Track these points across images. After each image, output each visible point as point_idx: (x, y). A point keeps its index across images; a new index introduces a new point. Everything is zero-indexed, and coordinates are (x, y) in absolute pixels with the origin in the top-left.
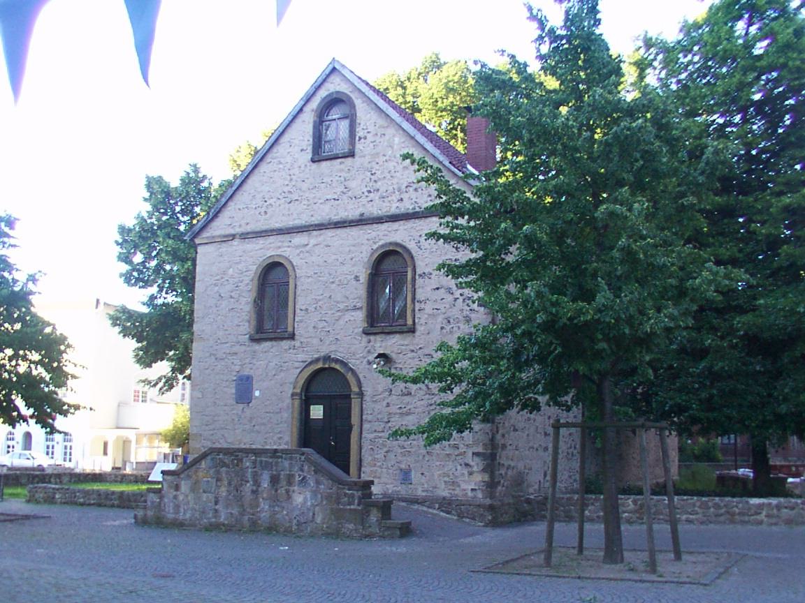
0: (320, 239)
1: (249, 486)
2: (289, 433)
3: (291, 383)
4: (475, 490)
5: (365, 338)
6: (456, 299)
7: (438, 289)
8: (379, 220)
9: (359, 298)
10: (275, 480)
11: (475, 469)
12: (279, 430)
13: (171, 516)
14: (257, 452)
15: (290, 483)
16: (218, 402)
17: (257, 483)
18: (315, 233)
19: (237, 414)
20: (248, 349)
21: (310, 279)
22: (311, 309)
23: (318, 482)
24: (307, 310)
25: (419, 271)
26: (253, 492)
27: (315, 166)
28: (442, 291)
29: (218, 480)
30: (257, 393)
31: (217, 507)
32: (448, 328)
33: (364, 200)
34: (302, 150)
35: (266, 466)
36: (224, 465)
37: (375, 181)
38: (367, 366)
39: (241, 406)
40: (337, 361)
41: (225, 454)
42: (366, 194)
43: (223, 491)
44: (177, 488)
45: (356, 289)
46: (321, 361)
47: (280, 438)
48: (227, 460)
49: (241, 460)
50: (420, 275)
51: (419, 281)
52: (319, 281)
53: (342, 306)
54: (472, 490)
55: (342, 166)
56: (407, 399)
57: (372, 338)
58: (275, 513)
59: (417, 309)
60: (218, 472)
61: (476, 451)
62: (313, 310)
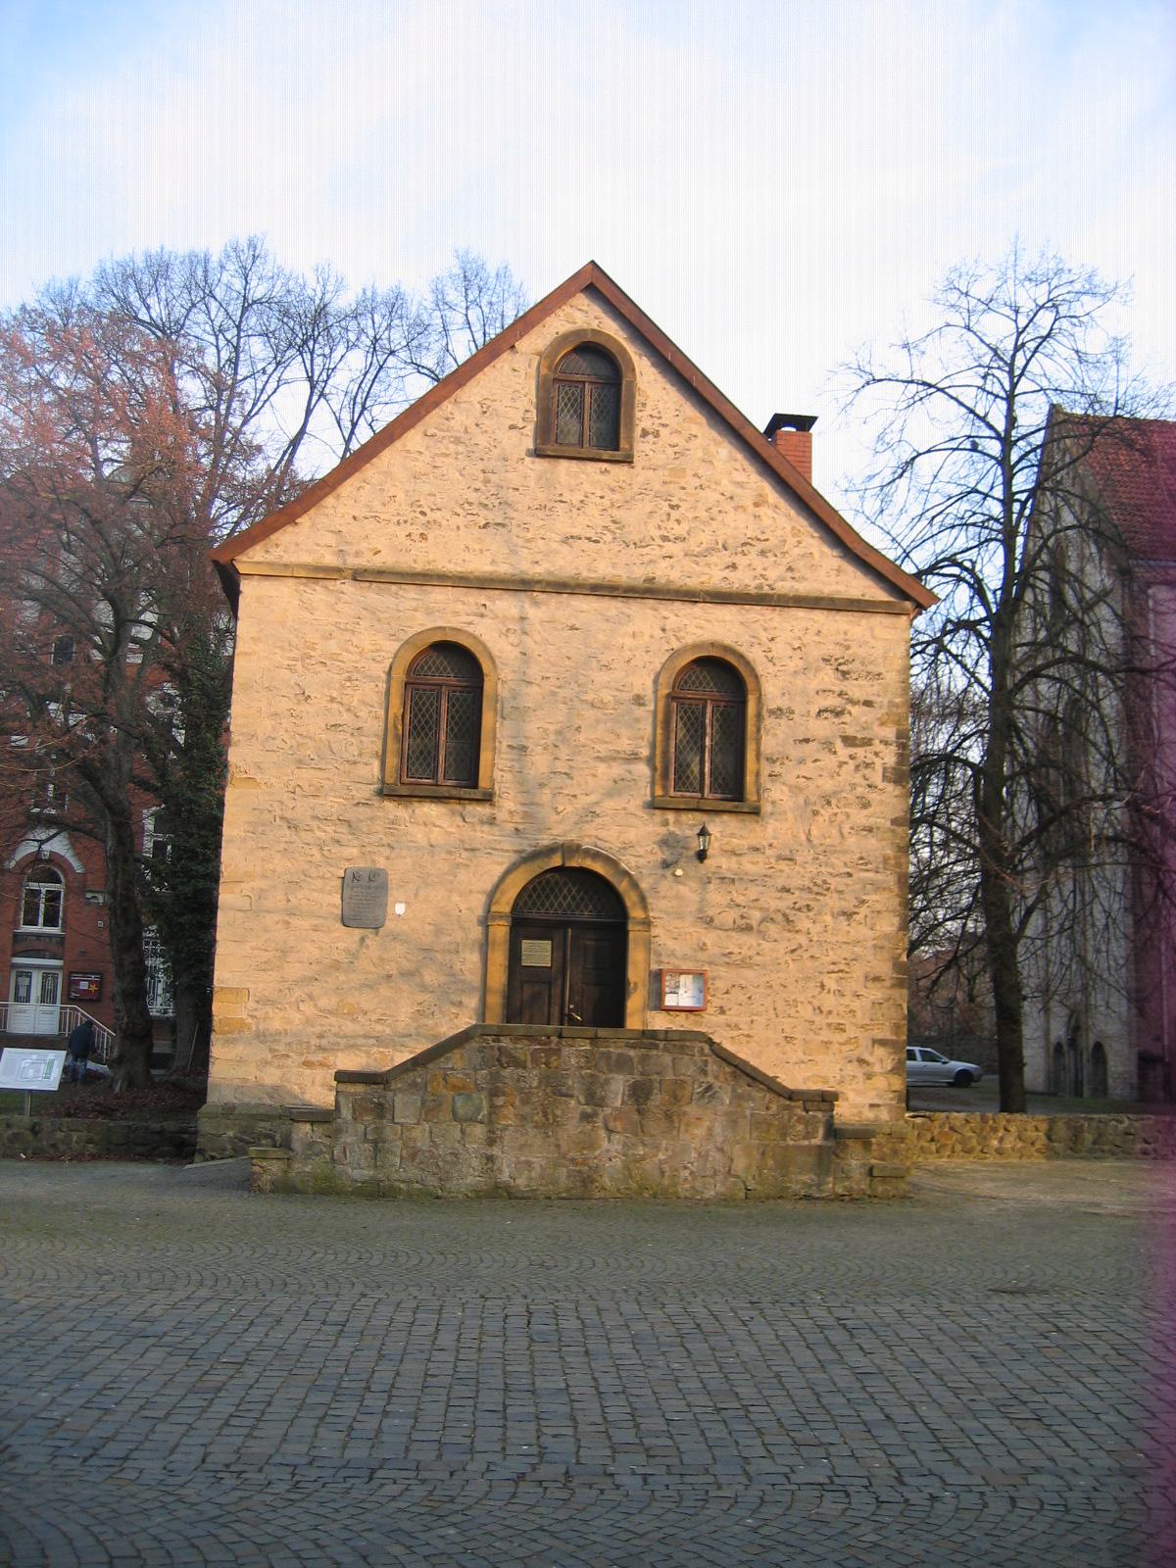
1: (575, 1106)
4: (878, 1106)
11: (877, 1068)
23: (738, 1098)
27: (541, 465)
31: (495, 1151)
34: (512, 427)
35: (622, 1064)
37: (678, 522)
49: (558, 1052)
50: (772, 712)
54: (872, 1106)
61: (880, 1036)
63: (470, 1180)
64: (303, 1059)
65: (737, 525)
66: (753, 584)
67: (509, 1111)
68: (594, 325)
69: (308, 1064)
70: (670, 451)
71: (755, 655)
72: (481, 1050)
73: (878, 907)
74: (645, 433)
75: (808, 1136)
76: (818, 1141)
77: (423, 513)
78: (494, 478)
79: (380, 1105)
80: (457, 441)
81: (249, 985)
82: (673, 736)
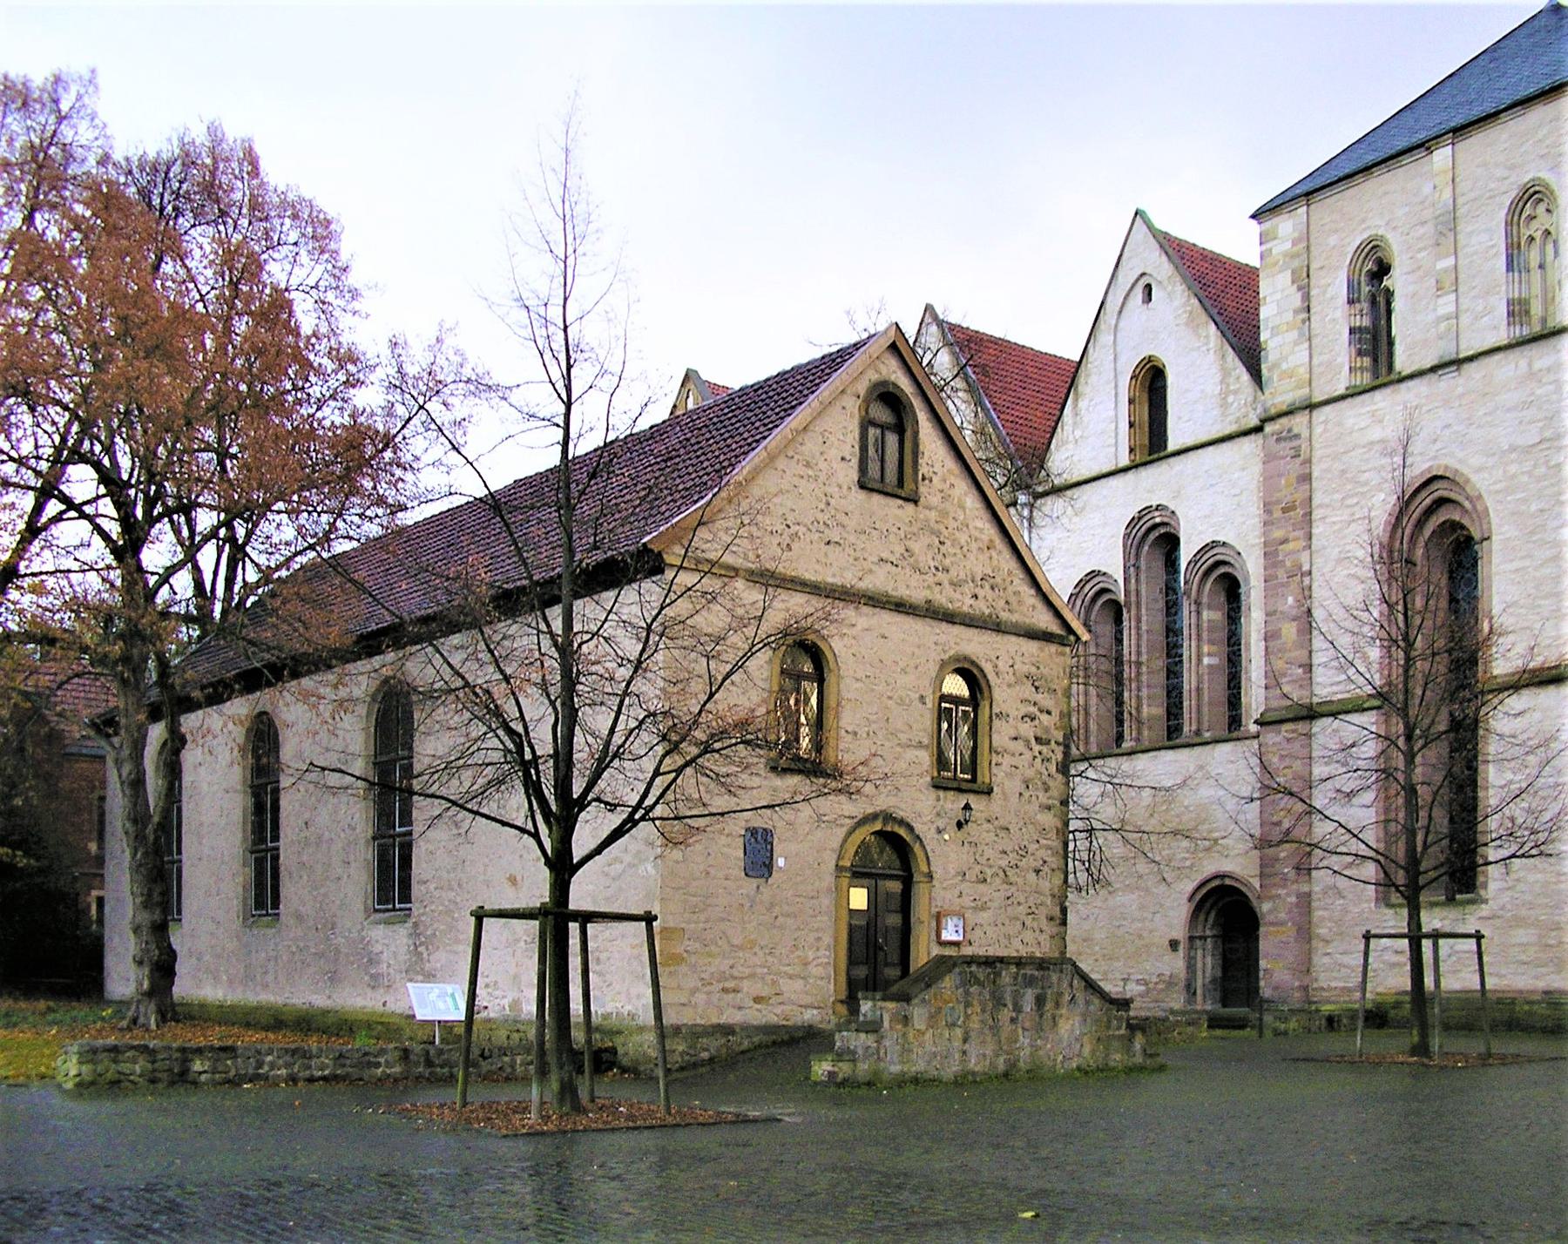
0: (874, 621)
2: (831, 932)
3: (832, 850)
5: (933, 794)
6: (1035, 757)
7: (1016, 739)
8: (950, 618)
9: (925, 730)
10: (1040, 1001)
12: (816, 926)
13: (895, 1069)
14: (1019, 962)
15: (1057, 1005)
16: (712, 871)
17: (1018, 1008)
18: (866, 609)
19: (748, 896)
20: (765, 783)
21: (859, 685)
22: (862, 733)
23: (1087, 1003)
24: (855, 734)
25: (996, 710)
26: (1013, 1020)
28: (1020, 742)
29: (968, 1005)
30: (781, 862)
31: (967, 1046)
32: (1026, 794)
33: (930, 579)
34: (843, 459)
35: (1030, 982)
36: (978, 982)
38: (936, 836)
39: (754, 882)
40: (902, 822)
41: (979, 964)
42: (933, 570)
43: (975, 1024)
44: (906, 1020)
45: (922, 716)
46: (881, 819)
47: (819, 939)
48: (981, 973)
50: (997, 715)
51: (996, 723)
52: (873, 690)
53: (903, 737)
55: (899, 512)
56: (981, 886)
57: (941, 793)
58: (1038, 1048)
59: (993, 763)
60: (967, 993)
62: (865, 735)
63: (954, 1069)
64: (721, 986)
65: (978, 564)
66: (987, 612)
67: (974, 1018)
68: (893, 378)
69: (725, 990)
70: (939, 495)
71: (988, 668)
72: (960, 974)
73: (1054, 866)
74: (924, 479)
75: (1119, 1028)
76: (1122, 1032)
77: (788, 526)
78: (832, 502)
79: (906, 1017)
80: (808, 465)
81: (683, 925)
82: (1082, 737)
